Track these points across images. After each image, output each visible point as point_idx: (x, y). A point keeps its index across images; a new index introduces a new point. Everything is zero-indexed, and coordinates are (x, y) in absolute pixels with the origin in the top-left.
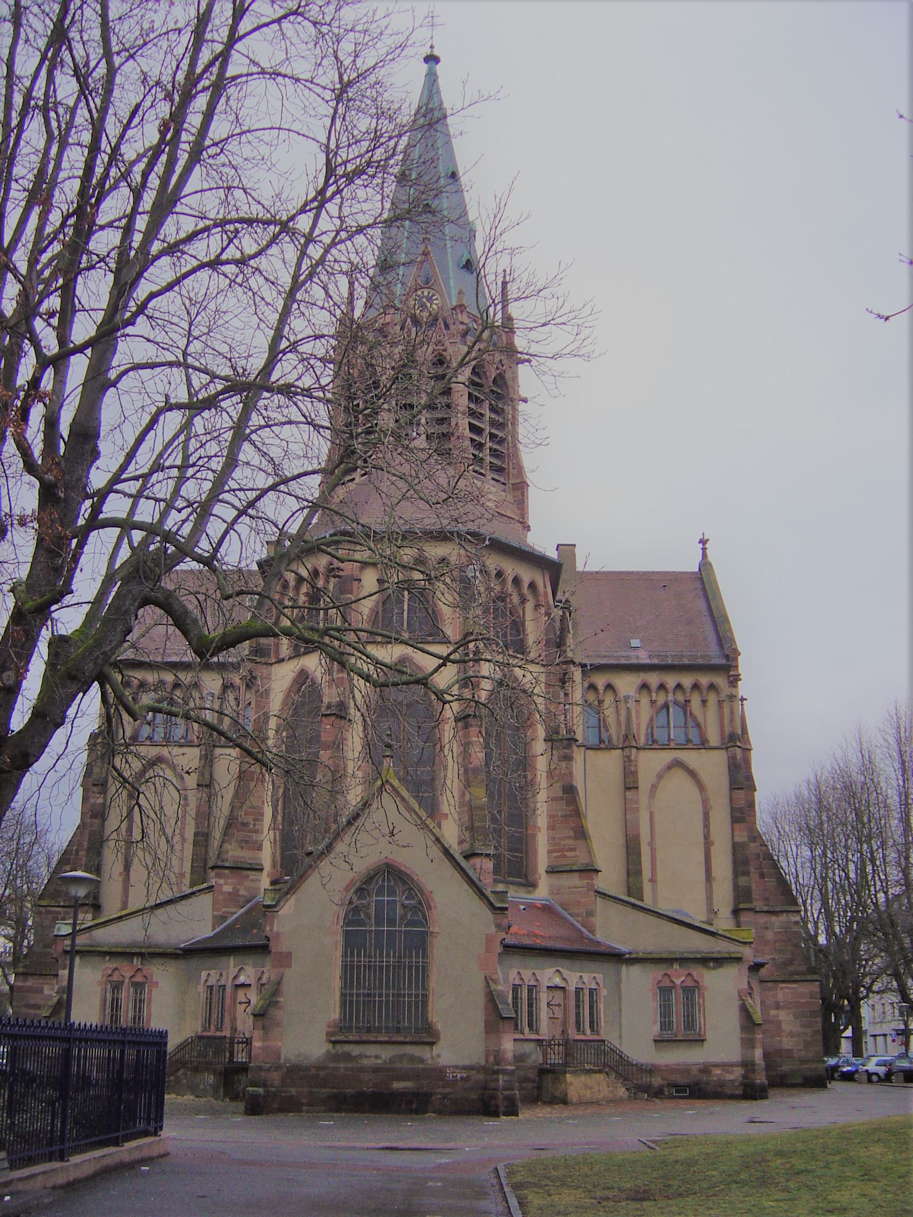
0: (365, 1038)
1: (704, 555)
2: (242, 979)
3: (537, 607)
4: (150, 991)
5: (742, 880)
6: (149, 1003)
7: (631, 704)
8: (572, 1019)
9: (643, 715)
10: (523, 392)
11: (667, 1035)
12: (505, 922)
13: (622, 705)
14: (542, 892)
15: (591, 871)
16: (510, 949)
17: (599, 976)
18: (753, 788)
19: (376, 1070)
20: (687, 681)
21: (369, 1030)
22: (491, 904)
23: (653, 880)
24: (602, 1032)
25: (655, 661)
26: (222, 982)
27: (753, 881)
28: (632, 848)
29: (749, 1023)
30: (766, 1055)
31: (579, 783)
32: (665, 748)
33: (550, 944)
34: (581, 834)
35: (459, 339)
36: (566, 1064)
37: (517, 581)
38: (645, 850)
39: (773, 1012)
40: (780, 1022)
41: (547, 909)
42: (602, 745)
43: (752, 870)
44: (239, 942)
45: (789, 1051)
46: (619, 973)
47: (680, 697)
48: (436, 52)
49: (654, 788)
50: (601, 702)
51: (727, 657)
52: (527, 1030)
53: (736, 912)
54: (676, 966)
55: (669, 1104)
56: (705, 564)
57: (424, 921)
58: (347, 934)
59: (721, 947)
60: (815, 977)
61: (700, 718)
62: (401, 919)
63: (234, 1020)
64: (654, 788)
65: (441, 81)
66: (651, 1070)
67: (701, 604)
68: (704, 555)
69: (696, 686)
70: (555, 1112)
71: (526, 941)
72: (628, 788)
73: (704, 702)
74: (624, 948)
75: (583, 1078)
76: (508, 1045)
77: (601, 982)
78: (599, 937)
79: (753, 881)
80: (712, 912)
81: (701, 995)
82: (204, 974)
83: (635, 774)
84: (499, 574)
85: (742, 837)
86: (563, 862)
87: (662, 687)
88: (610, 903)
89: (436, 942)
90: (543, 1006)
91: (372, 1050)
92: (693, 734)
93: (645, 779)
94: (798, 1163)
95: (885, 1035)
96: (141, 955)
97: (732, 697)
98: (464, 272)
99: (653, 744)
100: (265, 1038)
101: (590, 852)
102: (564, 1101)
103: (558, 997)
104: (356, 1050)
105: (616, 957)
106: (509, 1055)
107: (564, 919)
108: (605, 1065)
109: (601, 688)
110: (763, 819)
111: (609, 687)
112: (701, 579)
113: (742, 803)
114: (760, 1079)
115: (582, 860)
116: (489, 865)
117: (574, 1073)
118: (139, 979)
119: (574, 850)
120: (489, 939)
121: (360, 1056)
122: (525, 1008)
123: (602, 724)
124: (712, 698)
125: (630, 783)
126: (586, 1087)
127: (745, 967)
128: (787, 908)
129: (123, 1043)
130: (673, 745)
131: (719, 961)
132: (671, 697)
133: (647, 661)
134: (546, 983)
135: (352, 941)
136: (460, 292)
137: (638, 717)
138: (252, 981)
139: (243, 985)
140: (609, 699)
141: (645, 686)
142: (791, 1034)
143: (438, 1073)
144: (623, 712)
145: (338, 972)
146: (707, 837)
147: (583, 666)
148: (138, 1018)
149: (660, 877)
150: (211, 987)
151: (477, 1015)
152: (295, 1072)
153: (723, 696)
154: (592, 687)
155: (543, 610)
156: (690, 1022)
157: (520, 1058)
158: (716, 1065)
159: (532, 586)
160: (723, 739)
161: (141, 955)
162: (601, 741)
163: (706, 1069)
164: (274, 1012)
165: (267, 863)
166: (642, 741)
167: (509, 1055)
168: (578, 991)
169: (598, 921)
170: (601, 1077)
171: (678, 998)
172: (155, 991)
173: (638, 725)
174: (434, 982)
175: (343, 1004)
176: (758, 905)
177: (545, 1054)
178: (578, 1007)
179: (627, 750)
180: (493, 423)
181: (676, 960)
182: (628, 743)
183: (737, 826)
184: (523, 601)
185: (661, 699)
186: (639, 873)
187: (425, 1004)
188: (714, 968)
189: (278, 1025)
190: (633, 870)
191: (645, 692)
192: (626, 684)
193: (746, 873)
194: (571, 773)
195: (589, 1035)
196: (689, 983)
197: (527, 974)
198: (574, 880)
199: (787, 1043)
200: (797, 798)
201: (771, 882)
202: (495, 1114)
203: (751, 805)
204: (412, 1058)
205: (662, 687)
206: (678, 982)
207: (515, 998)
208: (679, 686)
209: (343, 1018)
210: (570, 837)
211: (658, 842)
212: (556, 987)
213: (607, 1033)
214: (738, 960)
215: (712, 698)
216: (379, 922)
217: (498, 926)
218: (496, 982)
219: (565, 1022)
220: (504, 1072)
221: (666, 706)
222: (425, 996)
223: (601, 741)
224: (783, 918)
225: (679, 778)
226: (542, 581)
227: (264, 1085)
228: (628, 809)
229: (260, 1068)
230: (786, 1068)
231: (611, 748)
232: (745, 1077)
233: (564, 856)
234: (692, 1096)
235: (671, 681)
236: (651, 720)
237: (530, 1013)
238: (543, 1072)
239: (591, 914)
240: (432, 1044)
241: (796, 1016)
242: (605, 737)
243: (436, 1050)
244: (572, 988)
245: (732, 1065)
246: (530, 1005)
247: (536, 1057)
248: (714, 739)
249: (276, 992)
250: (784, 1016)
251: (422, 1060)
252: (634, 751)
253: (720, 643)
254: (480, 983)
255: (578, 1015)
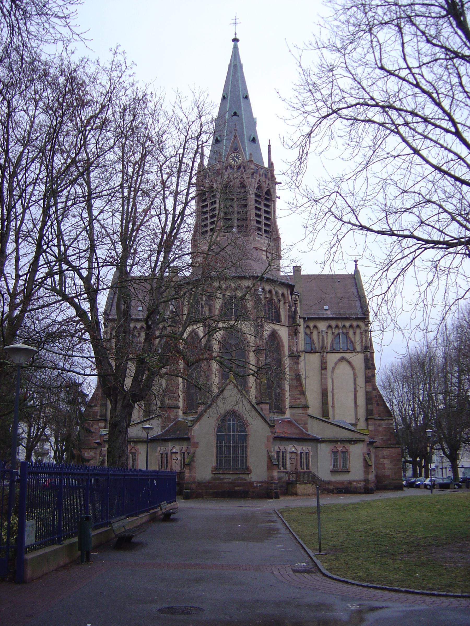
0: (225, 472)
1: (356, 267)
2: (174, 450)
3: (285, 303)
4: (138, 455)
5: (370, 407)
6: (138, 460)
7: (324, 334)
8: (299, 463)
9: (329, 339)
10: (278, 195)
11: (335, 470)
12: (274, 431)
13: (320, 334)
14: (288, 415)
15: (306, 407)
16: (275, 439)
17: (310, 448)
18: (374, 369)
19: (229, 483)
20: (347, 324)
21: (226, 469)
22: (269, 424)
23: (333, 407)
24: (311, 468)
25: (334, 316)
26: (166, 452)
27: (374, 407)
28: (324, 393)
29: (367, 466)
30: (376, 476)
31: (302, 371)
32: (338, 352)
33: (291, 436)
34: (303, 393)
35: (250, 176)
36: (297, 481)
37: (277, 293)
38: (330, 395)
39: (382, 460)
40: (384, 464)
41: (289, 422)
42: (312, 351)
43: (374, 402)
44: (173, 437)
45: (389, 475)
46: (317, 446)
47: (345, 331)
48: (238, 37)
49: (334, 368)
50: (311, 333)
51: (364, 314)
52: (282, 468)
53: (367, 419)
54: (339, 444)
55: (336, 495)
56: (357, 271)
57: (245, 431)
58: (217, 435)
59: (357, 436)
60: (399, 446)
61: (353, 339)
62: (237, 430)
63: (171, 466)
64: (334, 368)
65: (240, 51)
66: (329, 483)
67: (354, 290)
68: (356, 267)
69: (351, 326)
70: (293, 497)
71: (282, 435)
72: (323, 369)
73: (355, 333)
74: (319, 437)
75: (303, 486)
76: (276, 474)
77: (310, 449)
78: (309, 433)
79: (374, 407)
80: (357, 419)
81: (349, 455)
82: (159, 449)
83: (325, 363)
84: (270, 292)
85: (369, 389)
86: (295, 404)
87: (337, 326)
88: (314, 420)
89: (250, 438)
90: (288, 459)
91: (228, 476)
92: (350, 346)
93: (330, 365)
94: (356, 506)
95: (446, 468)
96: (134, 442)
97: (366, 331)
98: (252, 143)
99: (333, 351)
100: (190, 472)
101: (306, 400)
102: (296, 494)
103: (294, 456)
104: (222, 476)
105: (316, 441)
106: (276, 478)
107: (295, 425)
108: (311, 481)
109: (311, 327)
110: (379, 378)
111: (315, 327)
112: (355, 278)
113: (370, 375)
114: (371, 486)
115: (303, 403)
116: (267, 406)
117: (299, 484)
118: (133, 451)
119: (299, 399)
120: (268, 438)
121: (223, 479)
122: (282, 460)
123: (312, 342)
124: (358, 331)
125: (323, 367)
126: (304, 489)
127: (365, 444)
128: (387, 418)
129: (60, 474)
130: (341, 351)
131: (355, 442)
132: (341, 331)
133: (330, 316)
134: (289, 451)
135: (220, 438)
136: (251, 154)
137: (327, 339)
138: (178, 451)
139: (175, 453)
140: (315, 333)
141: (330, 326)
142: (389, 469)
143: (251, 484)
144: (321, 337)
145: (215, 449)
146: (355, 389)
147: (304, 318)
148: (133, 465)
149: (336, 405)
150: (162, 454)
151: (264, 463)
152: (201, 484)
153: (362, 330)
154: (308, 327)
155: (287, 304)
156: (344, 465)
157: (280, 479)
158: (354, 481)
159: (283, 295)
160: (362, 348)
161: (134, 442)
162: (312, 349)
163: (350, 482)
164: (193, 463)
165: (181, 404)
166: (329, 349)
167: (276, 478)
168: (301, 453)
169: (309, 426)
170: (310, 485)
171: (339, 455)
172: (139, 455)
173: (327, 343)
174: (249, 452)
175: (217, 460)
176: (376, 416)
177: (289, 477)
178: (301, 459)
179: (322, 353)
180: (266, 212)
181: (339, 441)
182: (323, 350)
183: (367, 384)
184: (279, 301)
185: (337, 332)
186: (327, 404)
187: (246, 460)
188: (354, 444)
189: (194, 468)
190: (325, 402)
191: (330, 329)
192: (322, 326)
193: (371, 404)
194: (299, 369)
195: (305, 470)
196: (344, 450)
197: (282, 448)
198: (300, 411)
199: (387, 472)
200: (402, 364)
201: (381, 407)
202: (271, 498)
203: (374, 376)
204: (242, 479)
205: (337, 326)
206: (340, 449)
207: (278, 456)
208: (344, 326)
209: (217, 465)
210: (297, 394)
211: (335, 391)
212: (293, 452)
213: (312, 469)
214: (363, 441)
215: (358, 331)
216: (229, 431)
217: (272, 432)
218: (271, 452)
219: (296, 466)
220: (274, 483)
221: (339, 334)
222: (246, 457)
223: (312, 349)
224: (386, 422)
225: (344, 366)
226: (287, 292)
227: (190, 489)
228: (323, 378)
229: (188, 483)
230: (387, 482)
231: (315, 352)
232: (365, 485)
233: (296, 402)
234: (345, 493)
235: (340, 324)
236: (332, 340)
237: (283, 462)
238: (288, 483)
239: (306, 424)
240: (249, 474)
241: (391, 462)
242: (313, 348)
243: (250, 476)
244: (299, 452)
245: (360, 481)
246: (283, 459)
247: (286, 478)
248: (358, 348)
249: (193, 457)
250: (386, 461)
251: (245, 480)
252: (325, 353)
253: (362, 307)
254: (266, 452)
255: (301, 462)
